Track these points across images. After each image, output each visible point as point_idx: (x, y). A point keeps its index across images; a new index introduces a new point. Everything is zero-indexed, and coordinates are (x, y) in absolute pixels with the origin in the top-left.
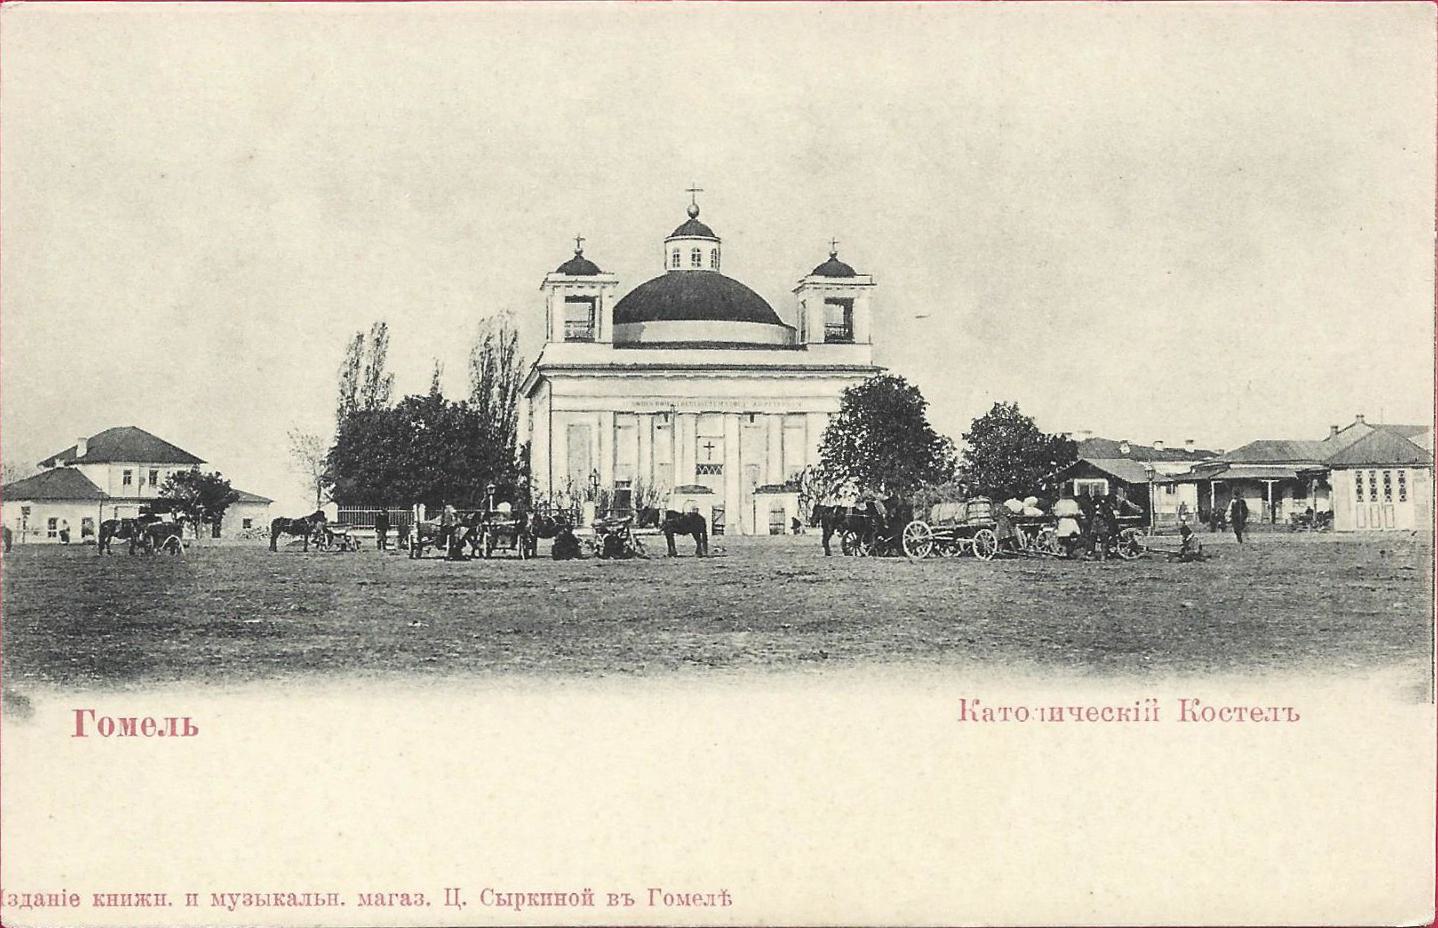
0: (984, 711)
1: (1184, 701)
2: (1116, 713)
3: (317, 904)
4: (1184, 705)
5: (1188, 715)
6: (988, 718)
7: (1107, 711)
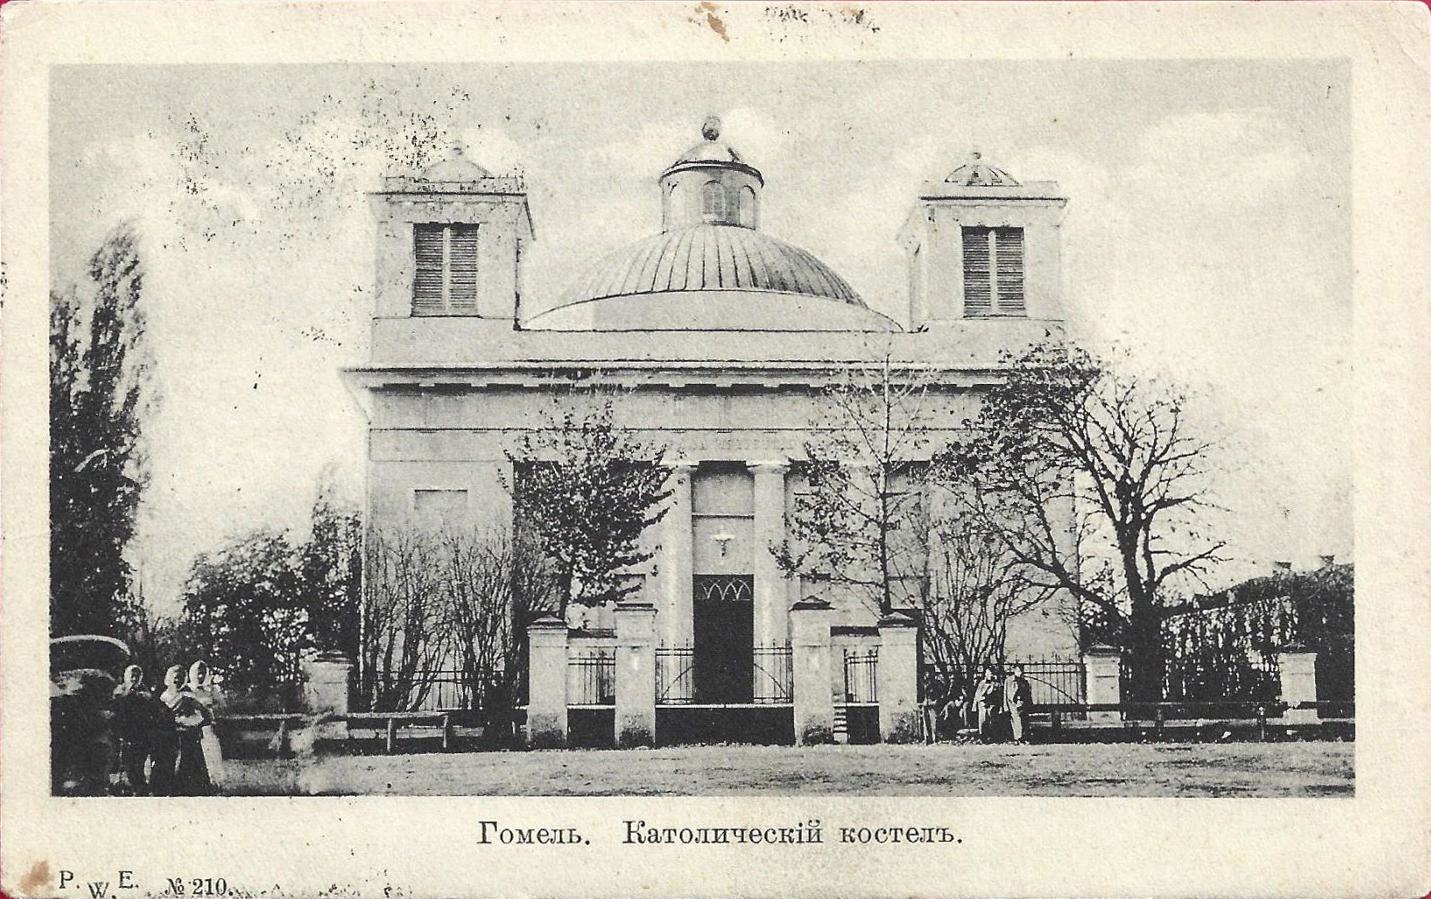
0: (650, 833)
1: (629, 823)
2: (779, 834)
3: (571, 841)
4: (629, 827)
5: (634, 837)
6: (653, 839)
7: (771, 832)
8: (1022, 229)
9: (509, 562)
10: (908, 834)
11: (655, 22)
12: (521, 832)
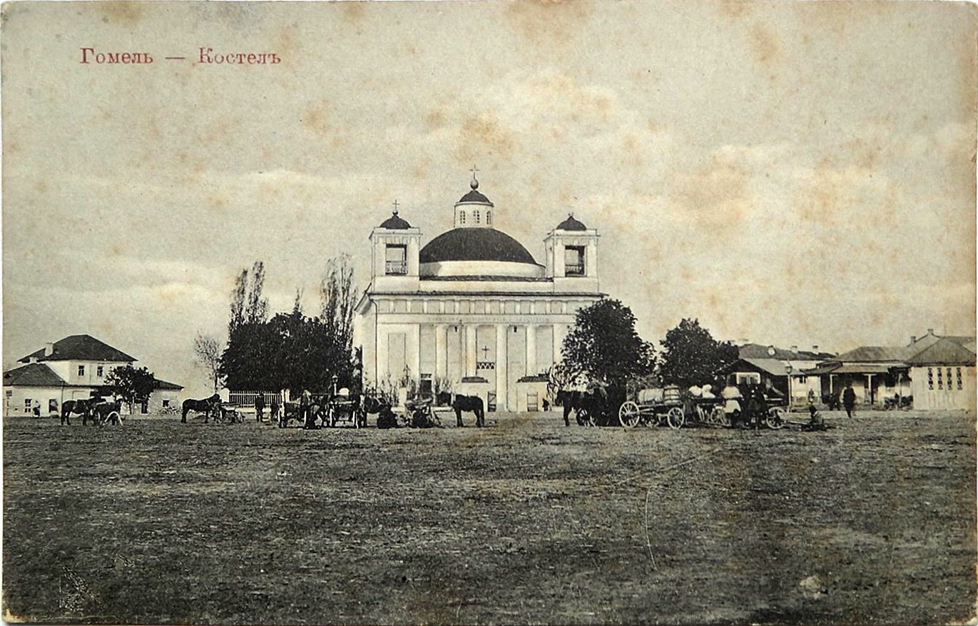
5: (205, 58)
8: (420, 279)
9: (959, 491)
10: (249, 58)
11: (323, 284)
12: (111, 55)
